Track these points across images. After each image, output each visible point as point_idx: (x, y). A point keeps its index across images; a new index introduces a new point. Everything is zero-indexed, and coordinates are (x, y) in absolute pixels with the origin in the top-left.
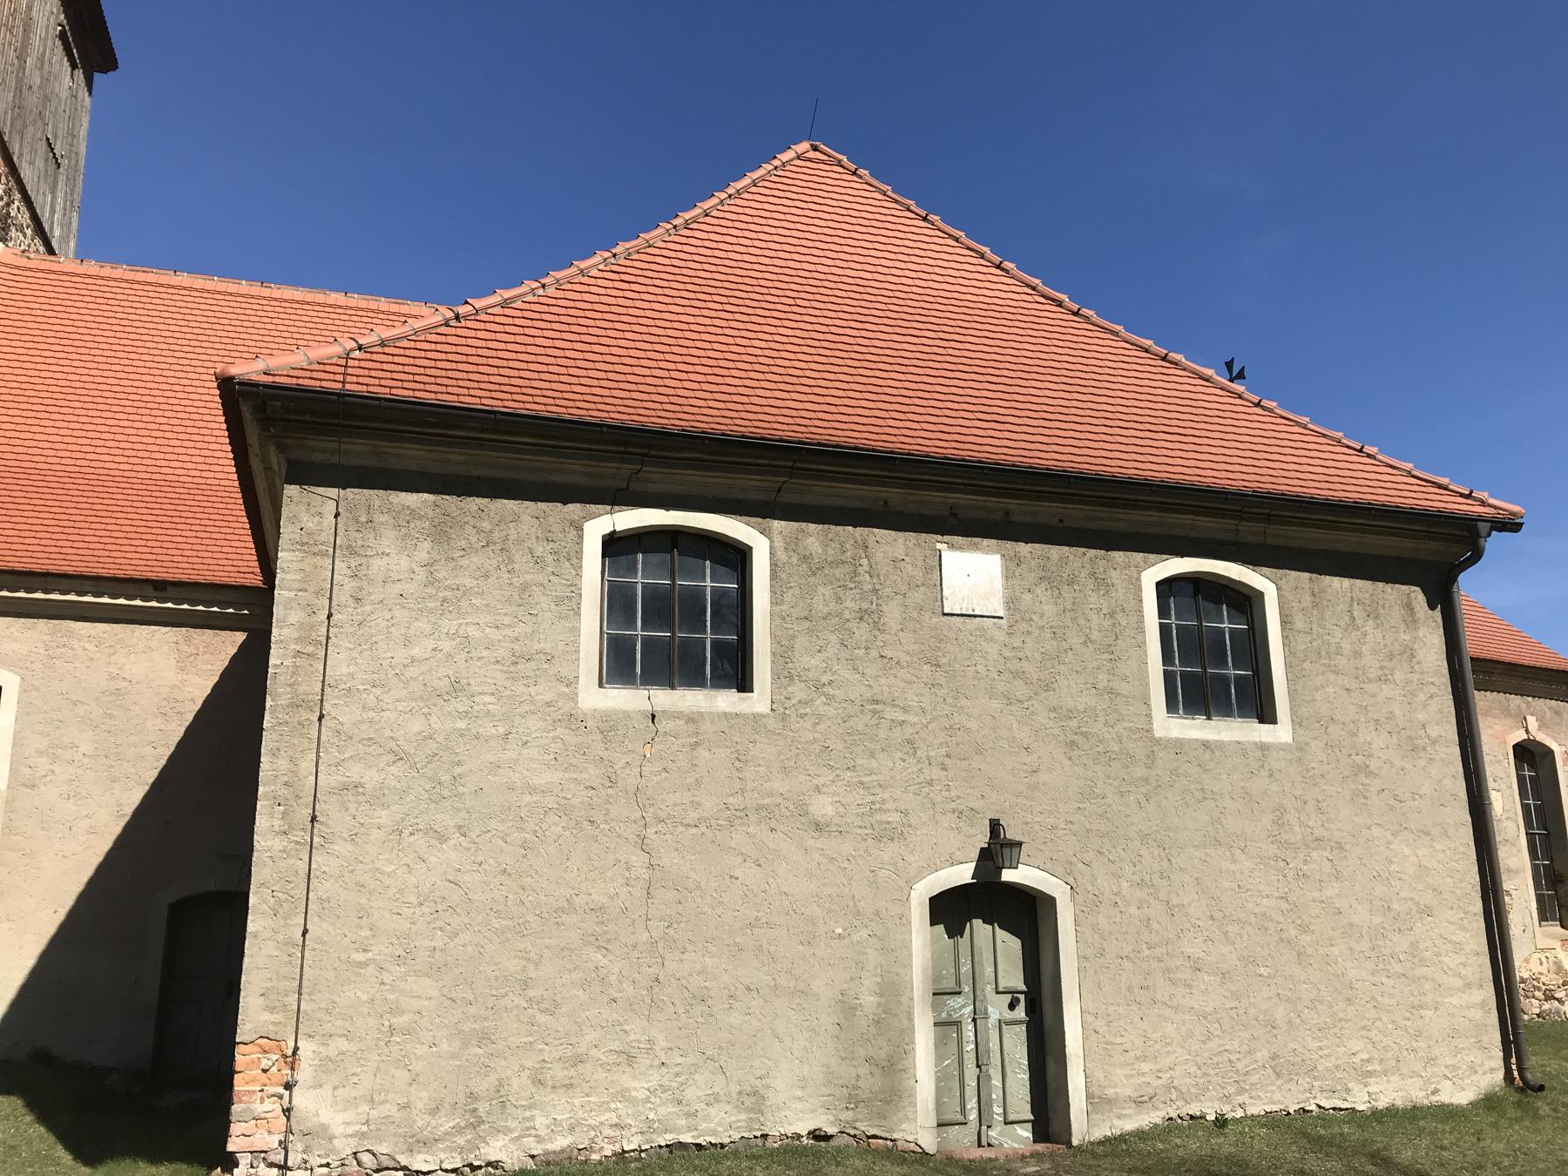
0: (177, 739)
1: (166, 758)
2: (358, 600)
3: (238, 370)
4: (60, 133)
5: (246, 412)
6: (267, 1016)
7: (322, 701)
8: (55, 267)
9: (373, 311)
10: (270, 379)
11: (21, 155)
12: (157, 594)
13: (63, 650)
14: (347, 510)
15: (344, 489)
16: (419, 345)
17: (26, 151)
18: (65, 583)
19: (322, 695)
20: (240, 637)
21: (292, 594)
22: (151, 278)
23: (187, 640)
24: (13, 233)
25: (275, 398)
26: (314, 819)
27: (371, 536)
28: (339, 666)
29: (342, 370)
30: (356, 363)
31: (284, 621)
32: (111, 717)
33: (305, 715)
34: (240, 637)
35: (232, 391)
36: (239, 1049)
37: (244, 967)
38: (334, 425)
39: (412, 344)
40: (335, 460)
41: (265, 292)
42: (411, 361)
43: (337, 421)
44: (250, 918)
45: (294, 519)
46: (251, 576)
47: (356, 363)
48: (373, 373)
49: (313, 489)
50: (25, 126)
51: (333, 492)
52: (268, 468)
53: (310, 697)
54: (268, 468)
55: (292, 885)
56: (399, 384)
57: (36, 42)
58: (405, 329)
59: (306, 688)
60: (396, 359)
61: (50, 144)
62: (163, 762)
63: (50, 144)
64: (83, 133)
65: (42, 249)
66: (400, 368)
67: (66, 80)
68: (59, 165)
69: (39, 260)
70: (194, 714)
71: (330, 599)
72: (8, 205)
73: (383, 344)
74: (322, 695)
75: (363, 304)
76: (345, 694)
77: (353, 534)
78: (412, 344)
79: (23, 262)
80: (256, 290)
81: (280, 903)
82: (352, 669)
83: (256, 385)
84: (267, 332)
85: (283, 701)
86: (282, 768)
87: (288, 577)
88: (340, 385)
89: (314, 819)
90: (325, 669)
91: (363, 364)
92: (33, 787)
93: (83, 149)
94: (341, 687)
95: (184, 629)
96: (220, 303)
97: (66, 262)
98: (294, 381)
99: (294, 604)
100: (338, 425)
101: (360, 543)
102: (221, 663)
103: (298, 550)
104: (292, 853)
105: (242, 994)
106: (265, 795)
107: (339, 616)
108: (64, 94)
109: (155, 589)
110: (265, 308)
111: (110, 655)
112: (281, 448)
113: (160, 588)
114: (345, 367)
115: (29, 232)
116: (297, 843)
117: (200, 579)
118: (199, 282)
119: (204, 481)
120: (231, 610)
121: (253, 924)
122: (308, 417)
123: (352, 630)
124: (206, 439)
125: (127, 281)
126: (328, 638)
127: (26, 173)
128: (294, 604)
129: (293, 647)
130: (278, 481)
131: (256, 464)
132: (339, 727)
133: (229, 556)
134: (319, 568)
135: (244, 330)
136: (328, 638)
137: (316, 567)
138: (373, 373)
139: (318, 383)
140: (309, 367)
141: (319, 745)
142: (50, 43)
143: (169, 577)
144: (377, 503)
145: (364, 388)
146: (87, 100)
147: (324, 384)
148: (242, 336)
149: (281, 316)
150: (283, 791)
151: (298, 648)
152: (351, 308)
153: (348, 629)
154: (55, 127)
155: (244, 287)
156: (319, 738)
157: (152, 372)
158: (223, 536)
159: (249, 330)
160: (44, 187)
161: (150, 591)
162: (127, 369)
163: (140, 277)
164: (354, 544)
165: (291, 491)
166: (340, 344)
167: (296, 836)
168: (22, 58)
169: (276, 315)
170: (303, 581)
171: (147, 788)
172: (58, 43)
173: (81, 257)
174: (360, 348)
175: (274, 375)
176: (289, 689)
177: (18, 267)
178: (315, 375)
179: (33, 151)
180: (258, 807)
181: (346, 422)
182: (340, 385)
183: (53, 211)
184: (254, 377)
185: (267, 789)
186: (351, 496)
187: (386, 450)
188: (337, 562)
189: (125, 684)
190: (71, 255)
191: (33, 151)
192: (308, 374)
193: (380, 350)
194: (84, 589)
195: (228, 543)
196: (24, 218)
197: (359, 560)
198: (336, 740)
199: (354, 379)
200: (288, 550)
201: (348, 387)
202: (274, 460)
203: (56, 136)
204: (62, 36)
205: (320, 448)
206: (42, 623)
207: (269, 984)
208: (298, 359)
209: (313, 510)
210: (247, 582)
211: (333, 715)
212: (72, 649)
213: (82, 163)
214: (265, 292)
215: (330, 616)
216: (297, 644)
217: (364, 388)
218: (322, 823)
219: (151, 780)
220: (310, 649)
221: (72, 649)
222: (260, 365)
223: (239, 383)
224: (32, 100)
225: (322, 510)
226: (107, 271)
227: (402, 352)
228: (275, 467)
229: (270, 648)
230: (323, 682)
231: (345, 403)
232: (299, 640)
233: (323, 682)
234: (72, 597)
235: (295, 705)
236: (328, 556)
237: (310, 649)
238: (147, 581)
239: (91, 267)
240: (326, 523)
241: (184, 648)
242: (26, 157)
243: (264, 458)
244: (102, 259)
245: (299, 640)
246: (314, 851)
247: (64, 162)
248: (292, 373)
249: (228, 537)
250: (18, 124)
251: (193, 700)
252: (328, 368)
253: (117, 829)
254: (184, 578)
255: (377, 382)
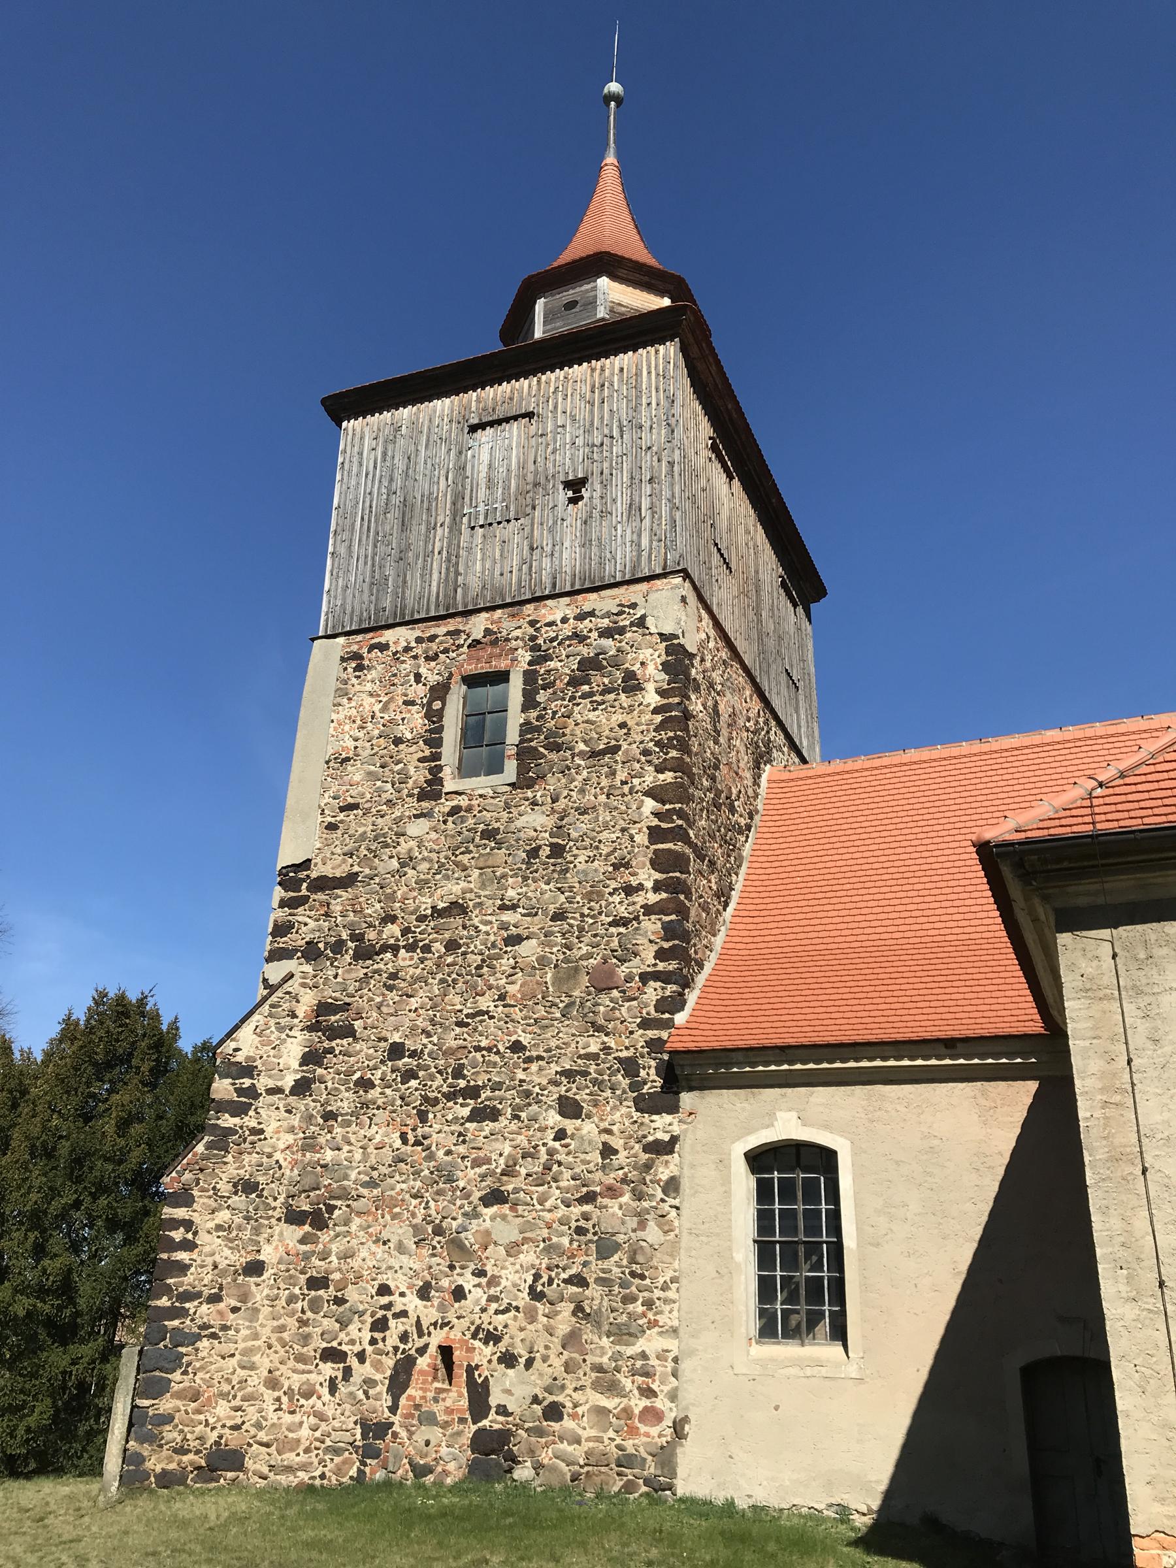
0: (993, 1195)
1: (987, 1214)
2: (1156, 1041)
3: (991, 834)
4: (794, 662)
5: (1006, 871)
6: (1157, 1508)
7: (1141, 1153)
8: (811, 773)
9: (1090, 738)
10: (1022, 835)
11: (770, 690)
12: (949, 1052)
13: (878, 1113)
14: (1124, 949)
15: (1115, 928)
16: (1159, 768)
17: (773, 684)
18: (871, 1051)
19: (1140, 1147)
20: (1033, 1086)
21: (1087, 1043)
22: (885, 761)
23: (984, 1093)
24: (775, 754)
25: (1032, 852)
26: (1161, 1284)
27: (1154, 972)
28: (1152, 1113)
29: (1088, 811)
30: (1101, 801)
31: (1084, 1072)
32: (930, 1174)
33: (1129, 1169)
34: (1033, 1086)
35: (989, 854)
36: (1136, 1542)
37: (1123, 1449)
38: (1093, 866)
39: (1152, 768)
40: (1100, 900)
41: (985, 747)
42: (1156, 785)
43: (1095, 862)
44: (1117, 1394)
45: (1072, 967)
46: (1032, 1023)
47: (1101, 801)
48: (1120, 807)
49: (1085, 933)
50: (769, 666)
51: (1105, 933)
52: (1036, 920)
53: (1128, 1150)
54: (1036, 920)
55: (1154, 1359)
56: (1150, 812)
57: (765, 596)
58: (1142, 755)
59: (1122, 1140)
60: (1140, 788)
61: (788, 674)
62: (985, 1218)
63: (788, 674)
64: (810, 656)
65: (797, 760)
66: (1146, 795)
67: (791, 616)
68: (797, 688)
69: (799, 771)
70: (1004, 1168)
71: (1126, 1043)
72: (768, 732)
73: (1122, 775)
74: (1140, 1147)
75: (1080, 734)
76: (1164, 1144)
77: (1136, 974)
78: (1152, 768)
79: (786, 775)
80: (977, 747)
81: (1145, 1378)
82: (1166, 1115)
83: (1012, 844)
84: (995, 784)
85: (1101, 1155)
86: (1115, 1227)
87: (1079, 1026)
88: (1091, 827)
89: (1161, 1284)
90: (1137, 1118)
91: (1107, 800)
92: (878, 1245)
93: (813, 670)
94: (1159, 1136)
95: (979, 1084)
96: (948, 768)
97: (817, 766)
98: (1046, 832)
99: (1091, 1053)
100: (1097, 866)
101: (1144, 981)
102: (1020, 1115)
103: (1084, 997)
104: (1147, 1322)
105: (1127, 1480)
106: (1103, 1256)
107: (1140, 1060)
108: (792, 630)
109: (946, 1047)
110: (988, 762)
111: (919, 1115)
112: (1045, 898)
113: (950, 1045)
114: (1091, 807)
115: (785, 749)
116: (1150, 1311)
117: (985, 1033)
118: (925, 754)
119: (967, 936)
120: (1019, 1060)
121: (1124, 1401)
122: (1065, 864)
123: (1156, 1074)
124: (961, 896)
125: (867, 770)
126: (1133, 1084)
127: (776, 703)
128: (1091, 1053)
129: (1099, 1097)
130: (1046, 931)
131: (1022, 918)
132: (1166, 1180)
133: (1007, 1007)
134: (1108, 1015)
135: (1001, 802)
136: (1133, 1084)
137: (1105, 1012)
138: (1120, 807)
139: (1068, 829)
140: (1056, 816)
141: (1148, 1201)
142: (775, 594)
143: (956, 1034)
144: (1153, 937)
145: (1115, 824)
146: (809, 628)
147: (1075, 829)
148: (973, 793)
149: (1005, 765)
150: (1122, 1253)
151: (1104, 1098)
152: (1069, 741)
153: (1151, 1073)
154: (790, 658)
155: (965, 747)
156: (1147, 1193)
157: (967, 875)
158: (996, 988)
159: (978, 787)
160: (790, 710)
161: (942, 1050)
162: (882, 846)
163: (877, 763)
164: (1138, 983)
165: (1064, 939)
166: (1081, 787)
167: (1146, 1303)
168: (758, 614)
169: (999, 766)
170: (1093, 1028)
171: (975, 1245)
172: (782, 591)
173: (827, 758)
174: (1101, 785)
175: (1025, 831)
176: (1104, 1142)
177: (783, 781)
178: (1063, 822)
179: (778, 683)
180: (1100, 1270)
181: (1104, 862)
182: (1091, 827)
183: (799, 727)
184: (1008, 837)
185: (1105, 1251)
186: (1125, 934)
187: (1152, 881)
188: (1125, 1005)
189: (936, 1142)
190: (818, 759)
191: (778, 683)
192: (1057, 823)
193: (1121, 782)
194: (886, 1054)
195: (1002, 994)
196: (780, 739)
197: (1148, 999)
198: (1166, 1195)
199: (1103, 817)
200: (1073, 999)
201: (1099, 826)
202: (1040, 911)
203: (792, 666)
204: (783, 585)
205: (1083, 893)
206: (858, 1089)
207: (1153, 1472)
208: (1043, 810)
209: (1089, 955)
210: (1029, 1031)
211: (1157, 1168)
212: (887, 1111)
213: (813, 680)
214: (985, 747)
215: (1129, 1062)
216: (1102, 1094)
217: (1115, 824)
218: (1172, 1289)
219: (978, 1237)
220: (1117, 1098)
221: (887, 1111)
222: (1011, 824)
223: (995, 846)
224: (771, 643)
225: (1098, 953)
226: (850, 765)
227: (1143, 778)
228: (1043, 917)
229: (1076, 1101)
230: (1138, 1131)
231: (1100, 843)
232: (1103, 1090)
233: (1138, 1131)
234: (878, 1063)
235: (1116, 1159)
236: (1114, 999)
237: (1117, 1098)
238: (938, 1040)
239: (837, 765)
240: (1105, 966)
241: (983, 1102)
242: (774, 691)
243: (1032, 913)
244: (844, 756)
245: (1103, 1090)
246: (1170, 1320)
247: (800, 684)
248: (1041, 825)
249: (1001, 987)
250: (764, 665)
251: (1000, 1154)
252: (1074, 812)
253: (956, 1287)
254: (970, 1034)
255: (1126, 815)
